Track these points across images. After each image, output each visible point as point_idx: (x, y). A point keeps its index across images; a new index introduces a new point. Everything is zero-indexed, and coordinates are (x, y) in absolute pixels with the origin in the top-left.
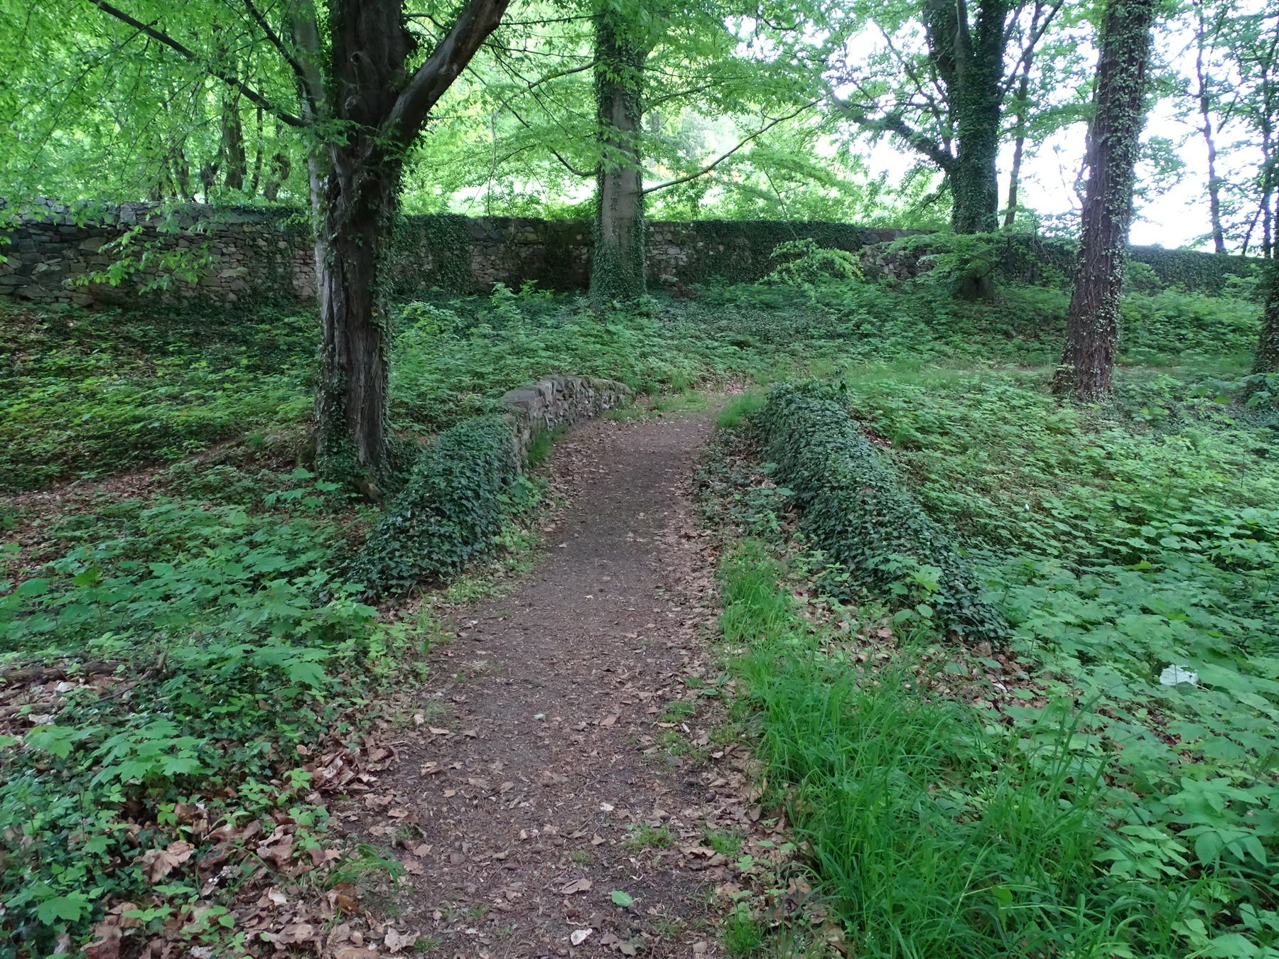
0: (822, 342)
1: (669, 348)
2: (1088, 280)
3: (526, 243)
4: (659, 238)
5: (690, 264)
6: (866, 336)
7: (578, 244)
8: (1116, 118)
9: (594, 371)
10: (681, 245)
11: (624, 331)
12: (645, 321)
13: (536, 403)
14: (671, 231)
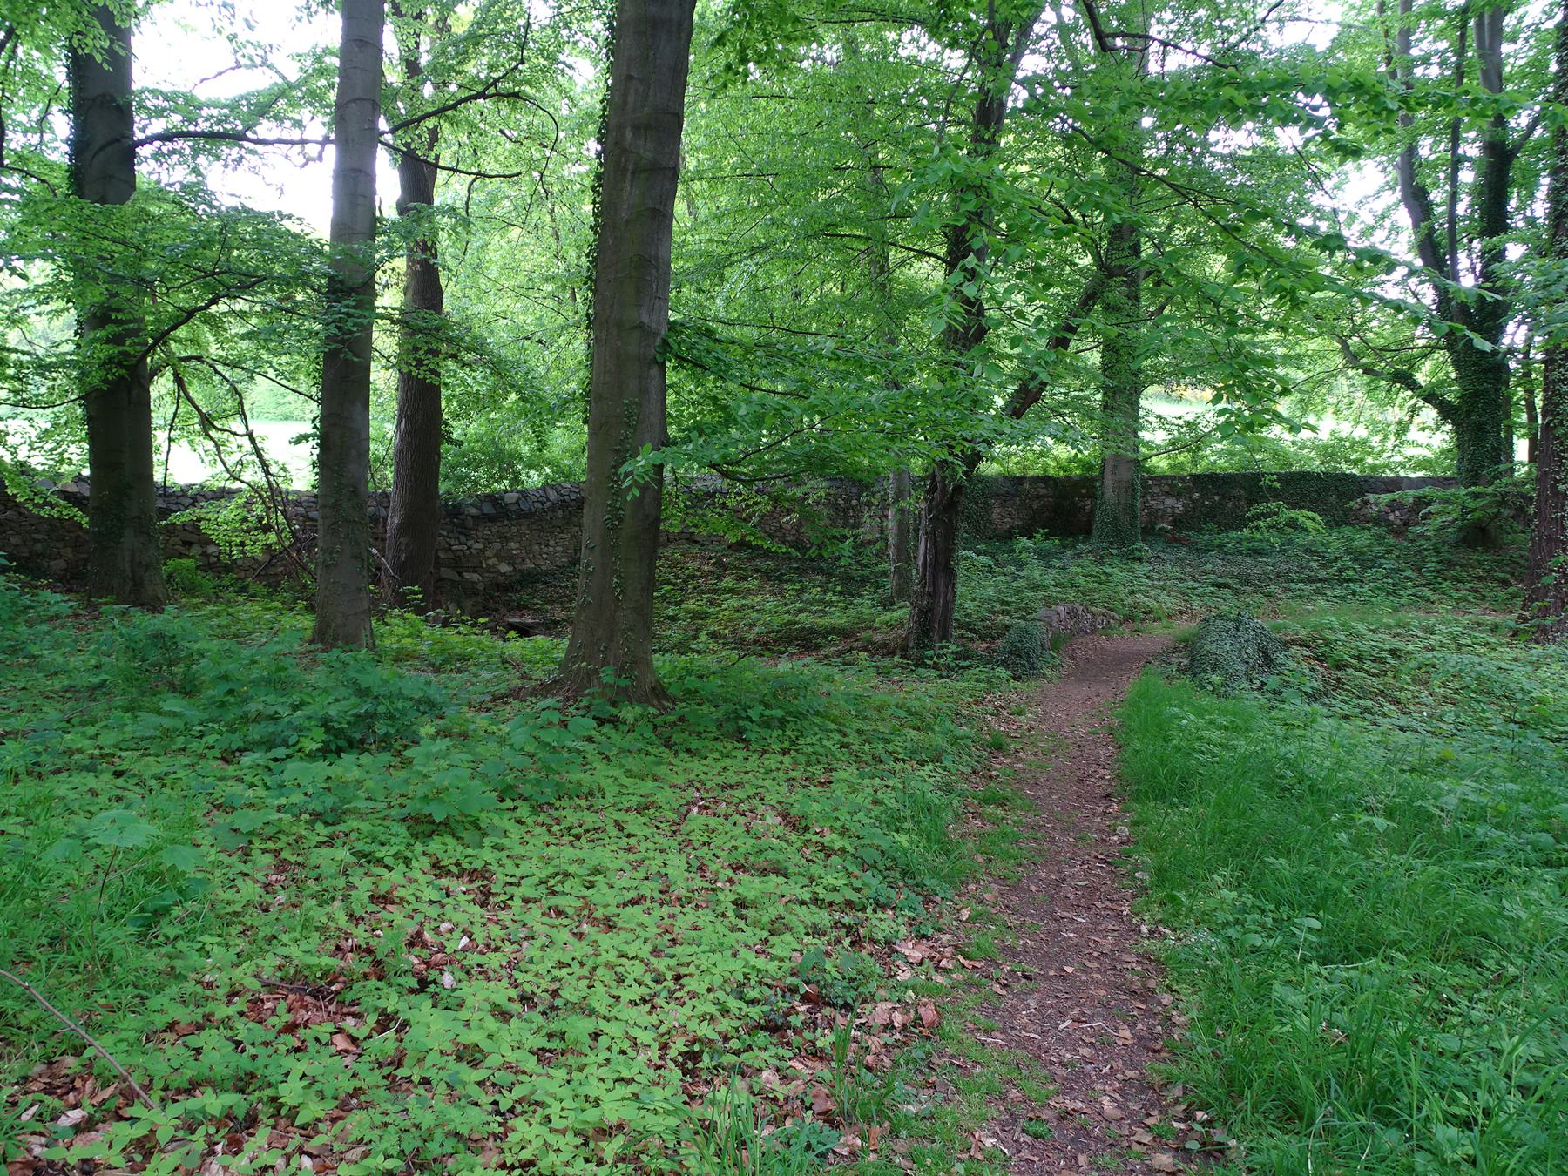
0: (1301, 585)
1: (1155, 587)
2: (1541, 538)
3: (1038, 497)
4: (1157, 490)
5: (1186, 512)
6: (1349, 581)
7: (1083, 496)
8: (1557, 405)
9: (1092, 603)
10: (1178, 496)
11: (1119, 575)
12: (1136, 565)
13: (1055, 618)
14: (1170, 484)
